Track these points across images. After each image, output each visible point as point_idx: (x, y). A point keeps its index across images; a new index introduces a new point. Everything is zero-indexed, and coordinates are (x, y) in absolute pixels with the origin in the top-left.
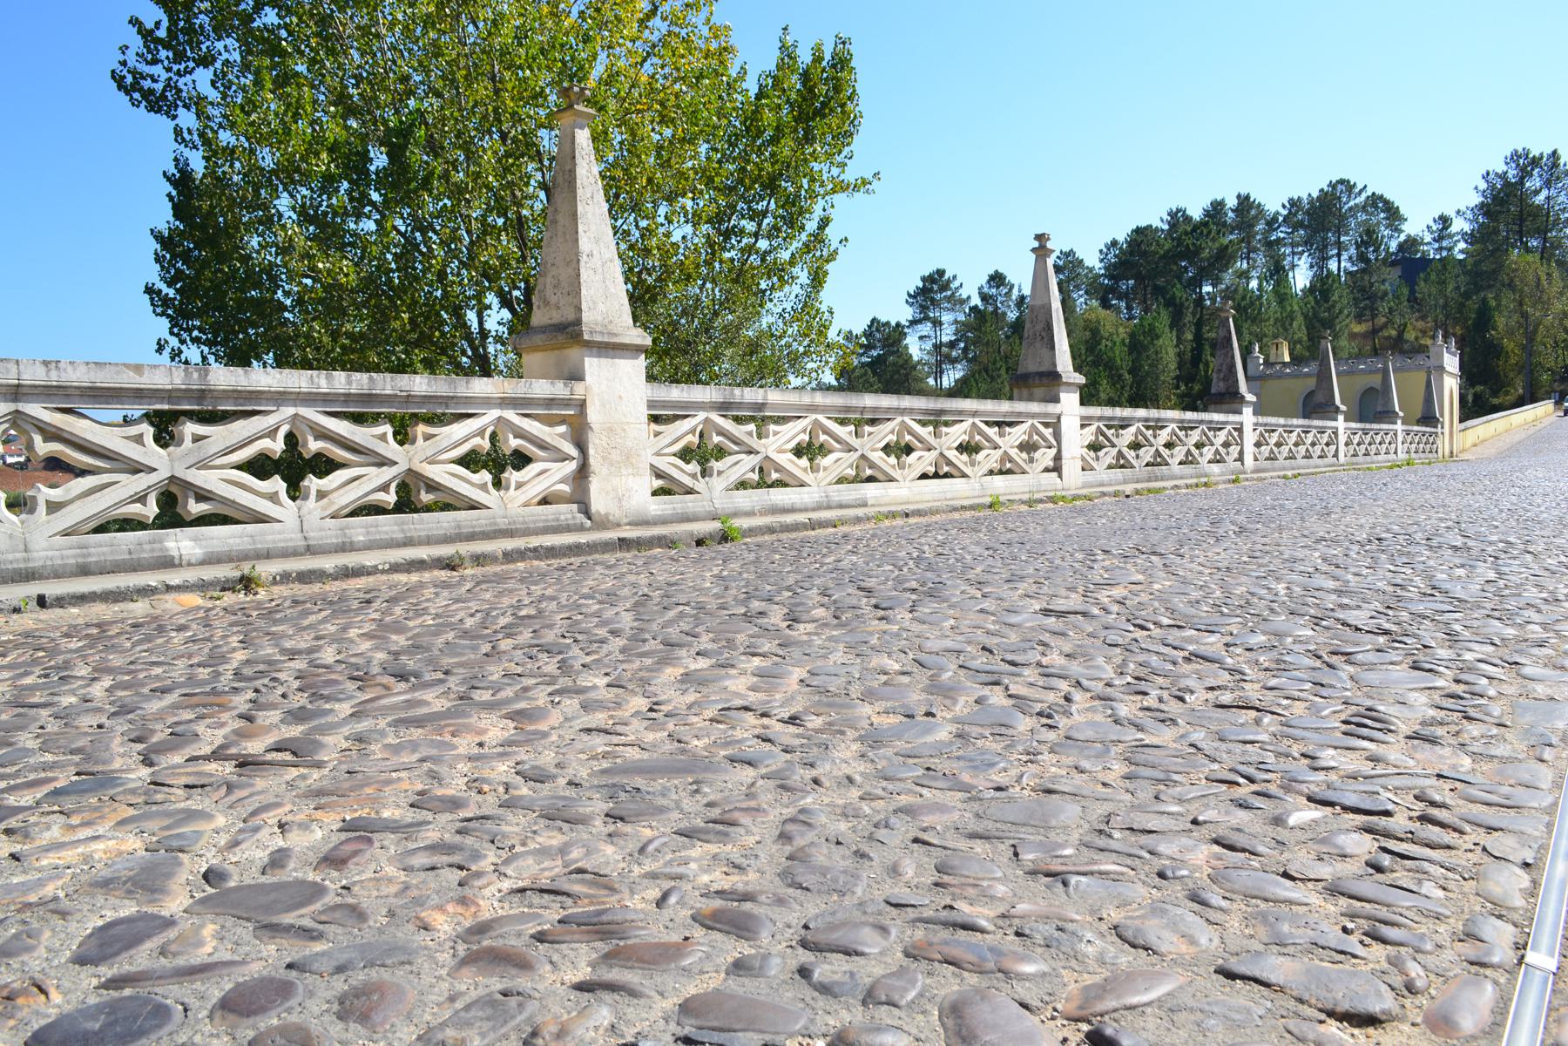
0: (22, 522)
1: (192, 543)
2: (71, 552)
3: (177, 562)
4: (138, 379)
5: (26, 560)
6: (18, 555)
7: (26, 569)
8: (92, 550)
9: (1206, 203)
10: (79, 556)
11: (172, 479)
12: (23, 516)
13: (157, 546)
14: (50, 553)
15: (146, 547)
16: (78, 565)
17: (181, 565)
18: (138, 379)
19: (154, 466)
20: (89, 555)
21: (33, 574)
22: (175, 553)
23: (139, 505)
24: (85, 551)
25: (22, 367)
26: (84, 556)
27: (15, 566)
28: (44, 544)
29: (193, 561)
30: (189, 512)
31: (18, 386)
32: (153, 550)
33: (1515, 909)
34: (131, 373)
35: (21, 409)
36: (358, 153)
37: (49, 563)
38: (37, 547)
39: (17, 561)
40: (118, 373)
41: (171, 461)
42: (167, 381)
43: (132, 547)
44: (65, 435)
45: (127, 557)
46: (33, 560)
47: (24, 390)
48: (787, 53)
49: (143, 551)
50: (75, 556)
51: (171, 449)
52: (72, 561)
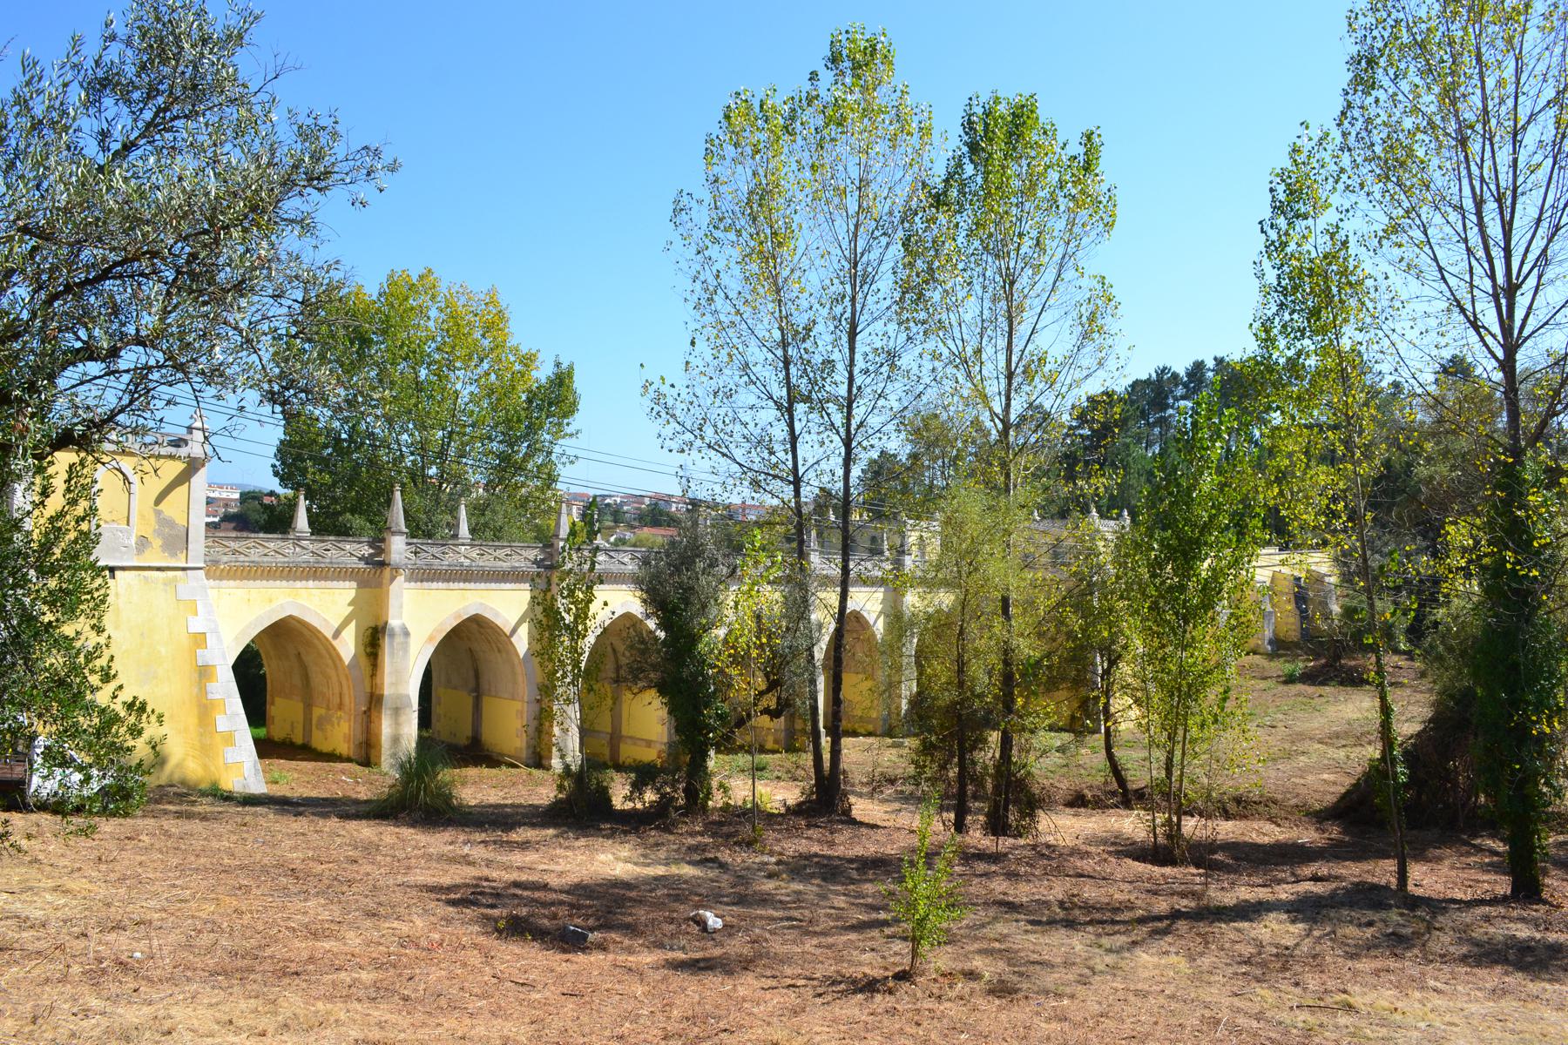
9: (1189, 363)
33: (649, 743)
48: (558, 365)
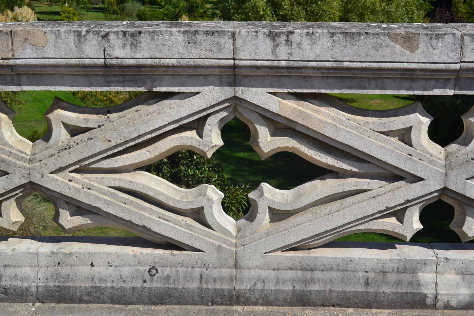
0: (239, 230)
1: (458, 278)
2: (291, 274)
3: (429, 301)
4: (408, 55)
5: (232, 279)
6: (225, 272)
7: (230, 291)
8: (318, 275)
10: (298, 280)
11: (445, 191)
12: (242, 221)
13: (405, 277)
14: (263, 273)
15: (391, 277)
16: (294, 293)
17: (434, 306)
18: (408, 55)
19: (423, 177)
20: (312, 281)
21: (238, 297)
22: (429, 291)
23: (393, 220)
24: (308, 275)
25: (239, 42)
26: (305, 282)
27: (218, 286)
28: (259, 261)
29: (454, 303)
30: (465, 235)
31: (234, 67)
32: (399, 283)
34: (398, 47)
35: (240, 95)
36: (464, 20)
37: (259, 286)
38: (249, 264)
39: (222, 279)
40: (378, 47)
41: (448, 167)
42: (454, 57)
43: (371, 275)
44: (298, 128)
45: (361, 289)
46: (241, 280)
47: (244, 72)
49: (385, 282)
50: (294, 281)
51: (453, 147)
52: (288, 287)
